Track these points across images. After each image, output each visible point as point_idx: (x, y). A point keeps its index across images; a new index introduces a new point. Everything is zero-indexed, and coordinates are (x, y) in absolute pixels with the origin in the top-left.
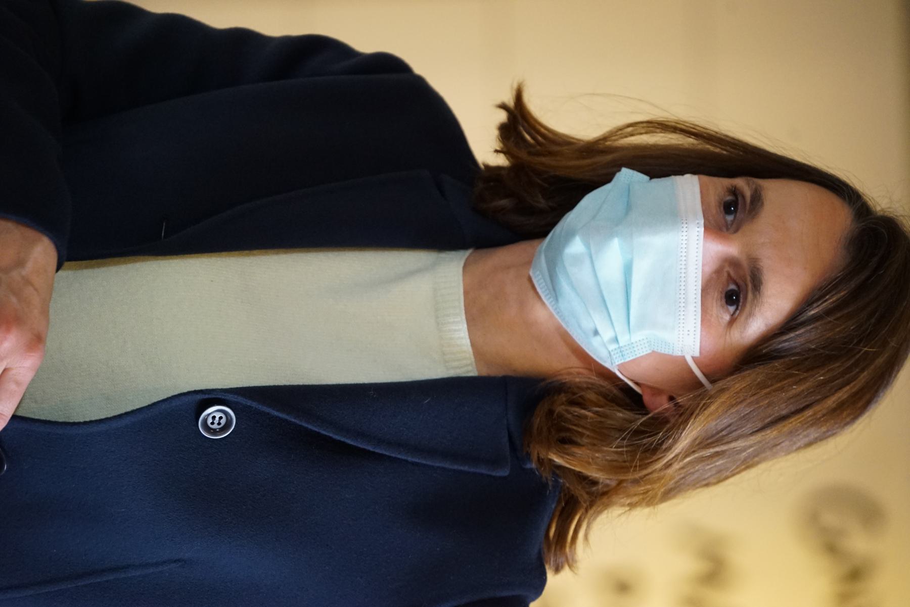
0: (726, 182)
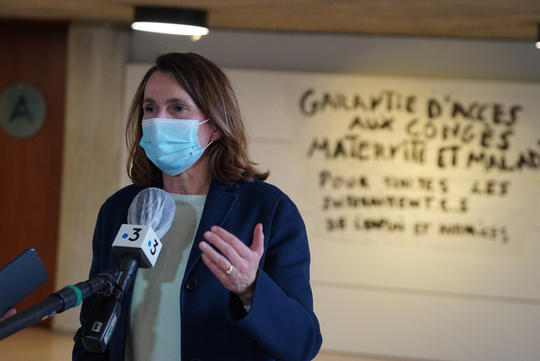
0: (145, 112)
